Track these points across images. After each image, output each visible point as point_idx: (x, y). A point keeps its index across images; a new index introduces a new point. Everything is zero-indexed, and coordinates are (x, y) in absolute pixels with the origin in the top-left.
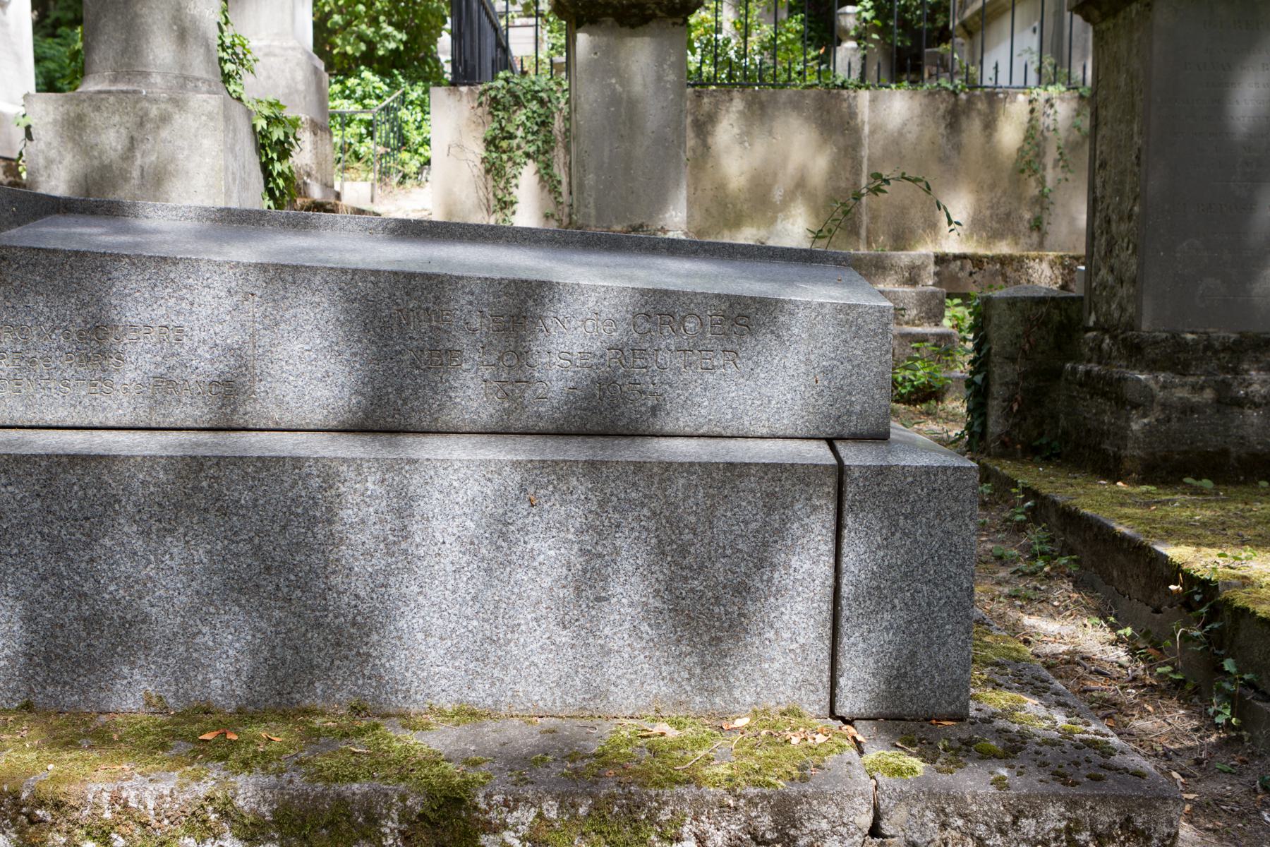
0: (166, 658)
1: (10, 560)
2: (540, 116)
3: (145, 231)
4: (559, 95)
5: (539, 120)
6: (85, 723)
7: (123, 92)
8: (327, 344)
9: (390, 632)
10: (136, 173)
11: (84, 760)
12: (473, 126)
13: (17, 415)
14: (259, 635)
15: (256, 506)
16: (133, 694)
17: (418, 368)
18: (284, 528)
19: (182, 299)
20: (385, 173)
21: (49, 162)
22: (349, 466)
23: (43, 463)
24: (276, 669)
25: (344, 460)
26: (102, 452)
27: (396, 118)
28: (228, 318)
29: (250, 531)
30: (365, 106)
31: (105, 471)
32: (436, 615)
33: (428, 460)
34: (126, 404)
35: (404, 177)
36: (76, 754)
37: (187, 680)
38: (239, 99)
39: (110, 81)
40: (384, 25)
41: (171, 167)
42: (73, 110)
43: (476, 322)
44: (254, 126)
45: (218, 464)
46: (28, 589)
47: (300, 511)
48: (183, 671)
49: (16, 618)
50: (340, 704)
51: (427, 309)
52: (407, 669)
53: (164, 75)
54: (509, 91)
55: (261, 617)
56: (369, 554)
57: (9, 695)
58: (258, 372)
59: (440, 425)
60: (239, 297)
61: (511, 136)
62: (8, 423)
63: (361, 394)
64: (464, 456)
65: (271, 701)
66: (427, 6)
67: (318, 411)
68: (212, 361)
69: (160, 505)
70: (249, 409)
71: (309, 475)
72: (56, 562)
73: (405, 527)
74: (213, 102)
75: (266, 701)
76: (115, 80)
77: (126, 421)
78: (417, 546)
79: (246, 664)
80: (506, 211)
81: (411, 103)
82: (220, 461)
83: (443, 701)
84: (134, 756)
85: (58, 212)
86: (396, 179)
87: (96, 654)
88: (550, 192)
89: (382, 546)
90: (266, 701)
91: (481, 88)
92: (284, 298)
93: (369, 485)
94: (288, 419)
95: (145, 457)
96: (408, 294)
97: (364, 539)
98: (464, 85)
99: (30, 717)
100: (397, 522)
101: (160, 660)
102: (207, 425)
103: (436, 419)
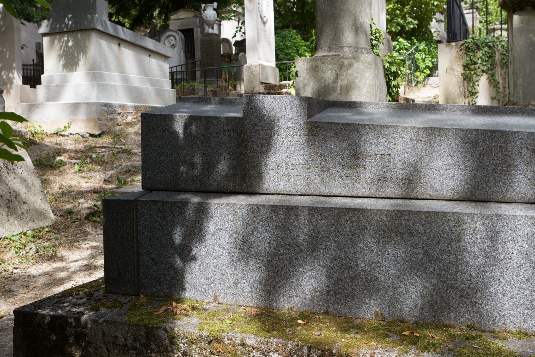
0: (385, 297)
1: (322, 251)
2: (489, 53)
3: (369, 114)
4: (498, 43)
5: (488, 55)
6: (351, 322)
7: (333, 55)
8: (454, 162)
9: (486, 293)
10: (338, 88)
11: (356, 338)
12: (458, 60)
13: (322, 191)
14: (425, 290)
15: (426, 233)
16: (369, 311)
17: (496, 173)
18: (438, 243)
19: (391, 143)
20: (410, 82)
21: (305, 85)
22: (468, 217)
23: (336, 211)
24: (433, 305)
25: (466, 214)
26: (360, 207)
27: (414, 58)
28: (410, 151)
29: (423, 244)
30: (400, 54)
31: (361, 216)
32: (509, 287)
33: (505, 215)
34: (366, 187)
35: (417, 83)
36: (352, 336)
37: (394, 307)
38: (378, 55)
39: (328, 51)
40: (408, 18)
41: (353, 85)
42: (314, 64)
43: (524, 152)
44: (384, 66)
45: (409, 214)
46: (328, 263)
47: (445, 236)
48: (392, 303)
49: (323, 275)
50: (462, 324)
51: (501, 146)
52: (494, 311)
53: (349, 47)
54: (474, 43)
55: (427, 282)
56: (477, 257)
57: (320, 307)
58: (423, 174)
59: (506, 199)
60: (415, 142)
61: (476, 63)
62: (318, 194)
63: (469, 184)
64: (522, 214)
65: (430, 320)
66: (426, 9)
67: (449, 191)
68: (403, 169)
69: (384, 231)
70: (419, 190)
71: (449, 220)
72: (340, 253)
73: (494, 245)
74: (370, 57)
75: (428, 319)
76: (330, 51)
77: (366, 194)
78: (500, 254)
79: (420, 302)
80: (473, 97)
81: (420, 51)
82: (410, 212)
83: (511, 327)
84: (376, 339)
85: (330, 107)
86: (414, 83)
87: (355, 293)
88: (494, 87)
89: (483, 253)
90: (428, 319)
91: (461, 43)
92: (435, 142)
93: (478, 226)
94: (435, 195)
95: (378, 210)
96: (491, 140)
97: (474, 250)
98: (453, 42)
99: (328, 317)
100: (490, 243)
101: (382, 297)
102: (400, 197)
103: (505, 196)
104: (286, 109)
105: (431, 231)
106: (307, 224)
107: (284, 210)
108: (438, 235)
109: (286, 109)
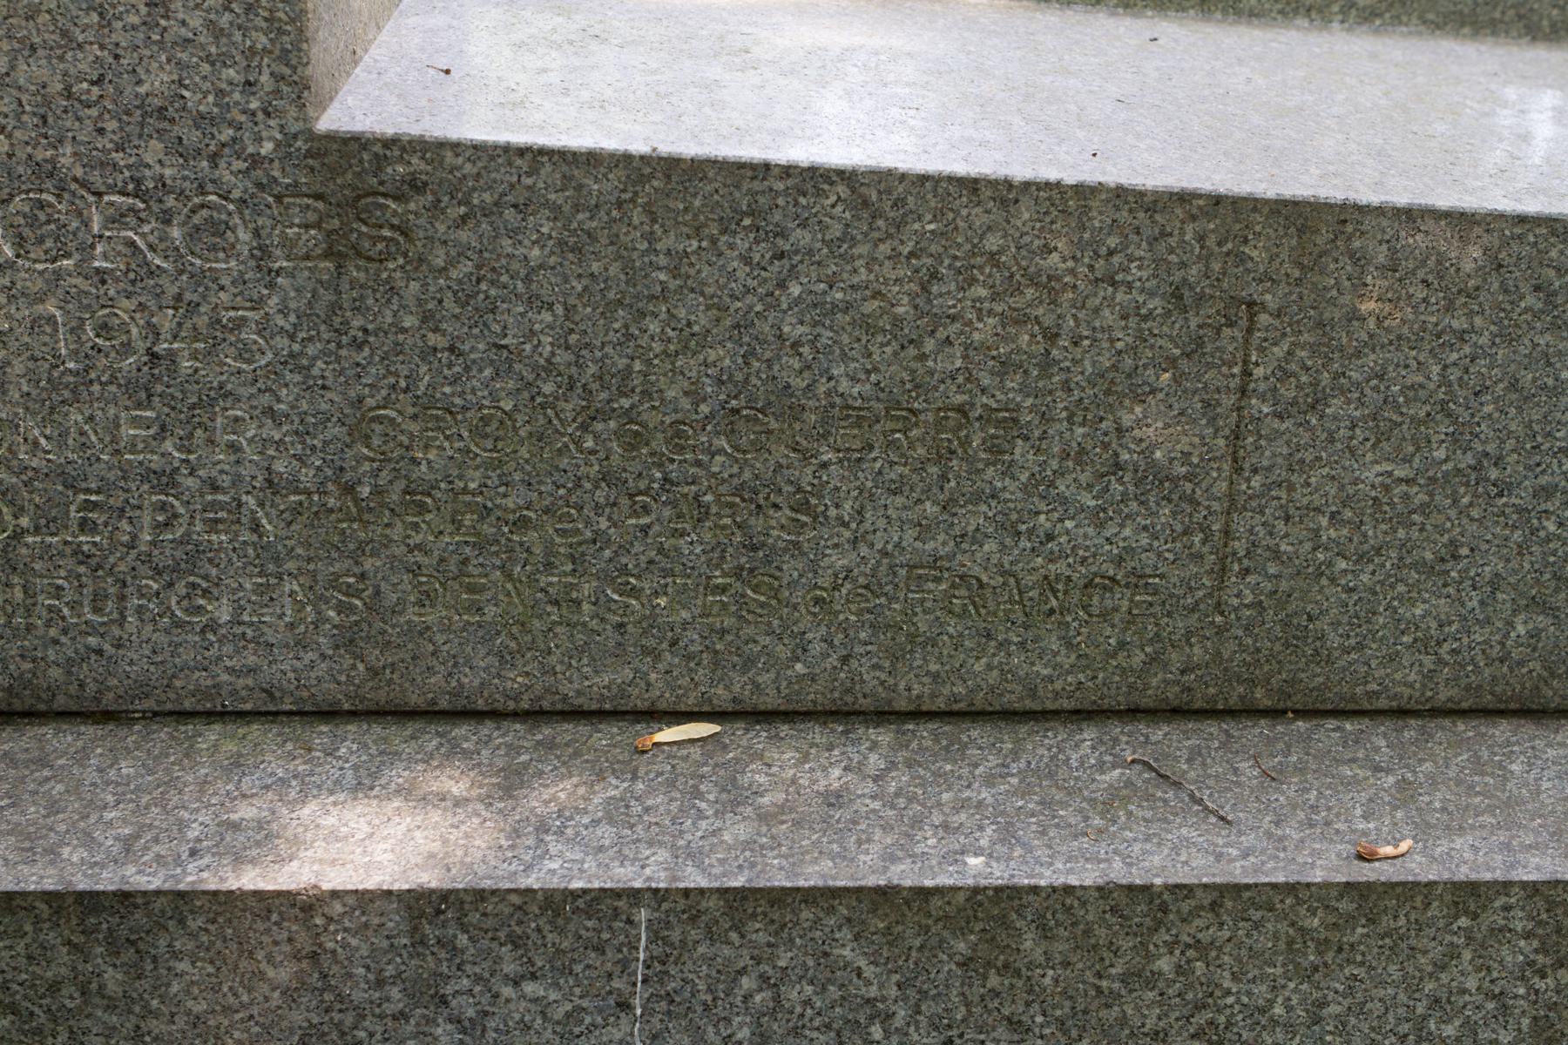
13: (470, 680)
15: (1317, 1020)
19: (1022, 320)
34: (817, 648)
58: (1240, 546)
104: (106, 23)
105: (1361, 1010)
106: (401, 1016)
107: (194, 924)
108: (1405, 1028)
109: (106, 23)
